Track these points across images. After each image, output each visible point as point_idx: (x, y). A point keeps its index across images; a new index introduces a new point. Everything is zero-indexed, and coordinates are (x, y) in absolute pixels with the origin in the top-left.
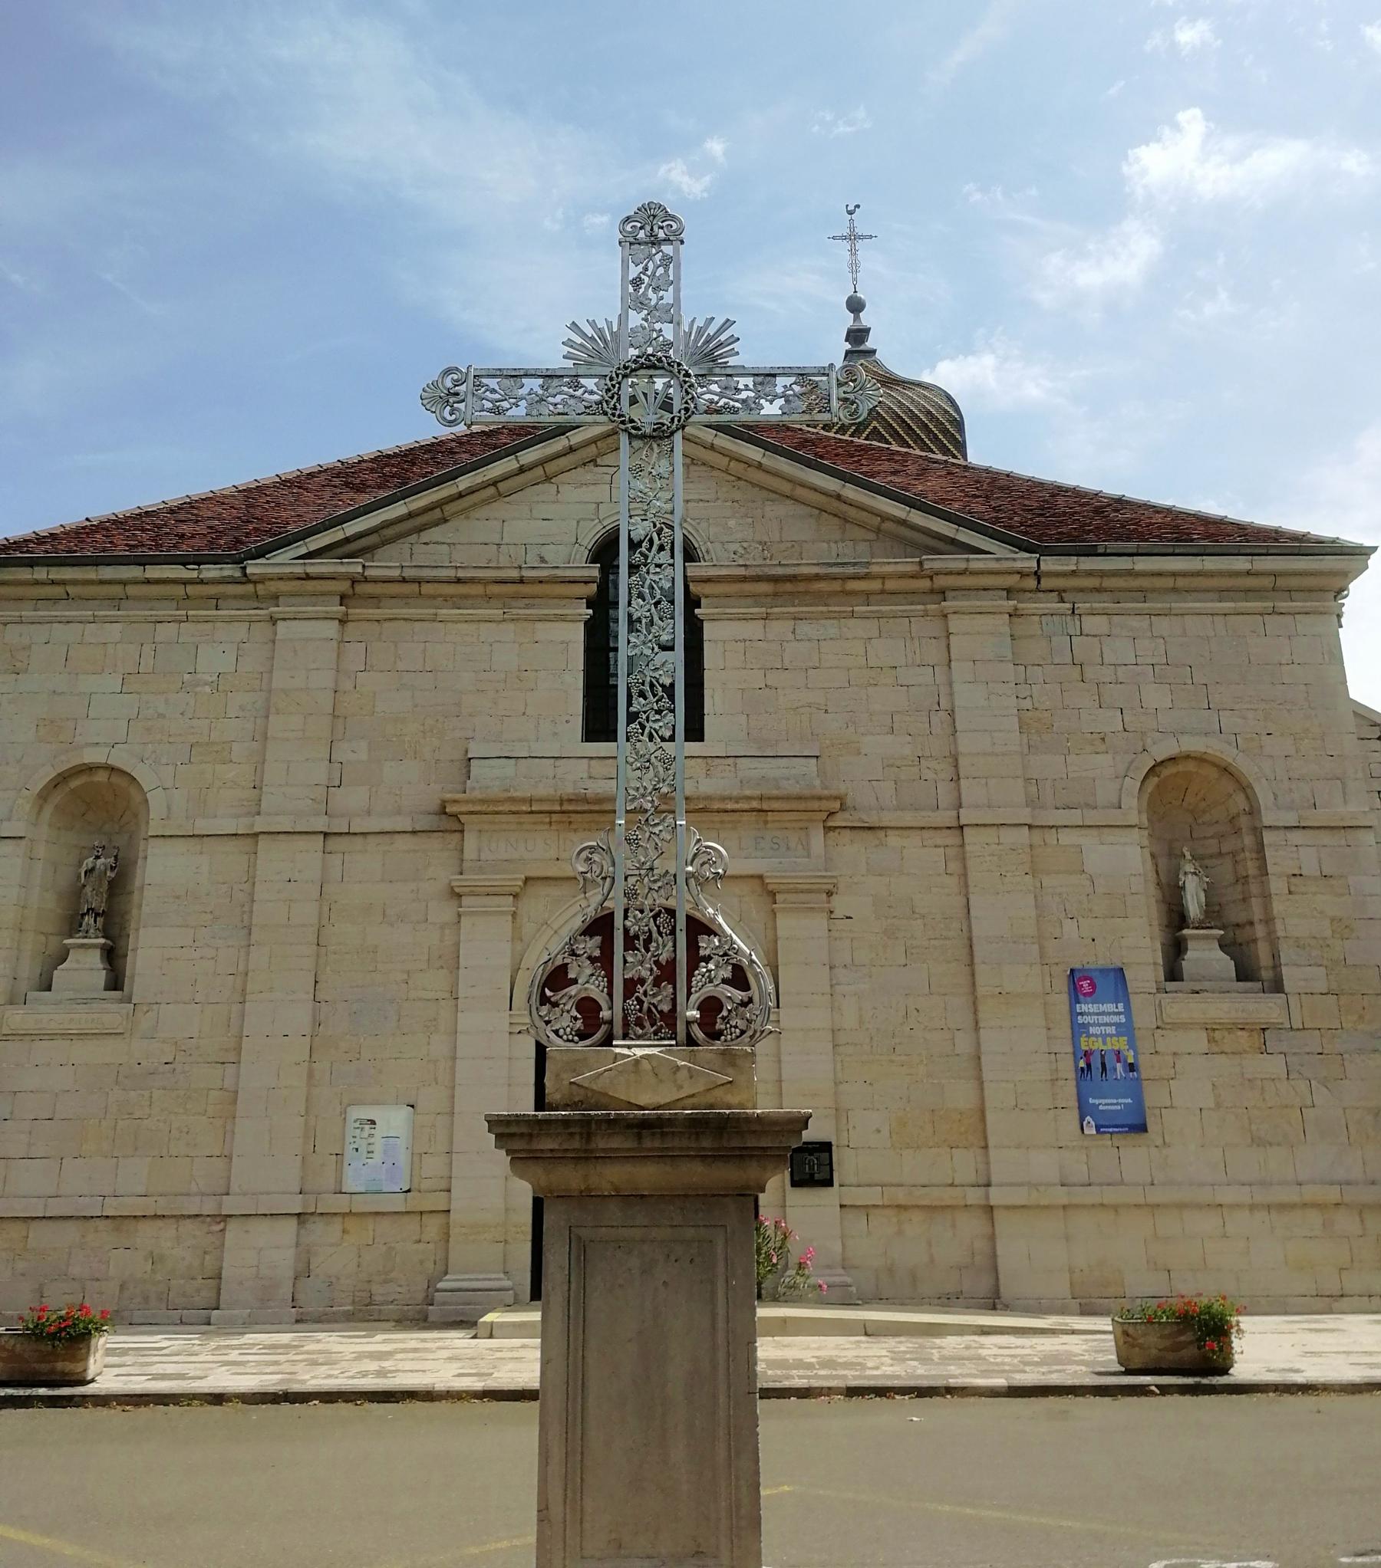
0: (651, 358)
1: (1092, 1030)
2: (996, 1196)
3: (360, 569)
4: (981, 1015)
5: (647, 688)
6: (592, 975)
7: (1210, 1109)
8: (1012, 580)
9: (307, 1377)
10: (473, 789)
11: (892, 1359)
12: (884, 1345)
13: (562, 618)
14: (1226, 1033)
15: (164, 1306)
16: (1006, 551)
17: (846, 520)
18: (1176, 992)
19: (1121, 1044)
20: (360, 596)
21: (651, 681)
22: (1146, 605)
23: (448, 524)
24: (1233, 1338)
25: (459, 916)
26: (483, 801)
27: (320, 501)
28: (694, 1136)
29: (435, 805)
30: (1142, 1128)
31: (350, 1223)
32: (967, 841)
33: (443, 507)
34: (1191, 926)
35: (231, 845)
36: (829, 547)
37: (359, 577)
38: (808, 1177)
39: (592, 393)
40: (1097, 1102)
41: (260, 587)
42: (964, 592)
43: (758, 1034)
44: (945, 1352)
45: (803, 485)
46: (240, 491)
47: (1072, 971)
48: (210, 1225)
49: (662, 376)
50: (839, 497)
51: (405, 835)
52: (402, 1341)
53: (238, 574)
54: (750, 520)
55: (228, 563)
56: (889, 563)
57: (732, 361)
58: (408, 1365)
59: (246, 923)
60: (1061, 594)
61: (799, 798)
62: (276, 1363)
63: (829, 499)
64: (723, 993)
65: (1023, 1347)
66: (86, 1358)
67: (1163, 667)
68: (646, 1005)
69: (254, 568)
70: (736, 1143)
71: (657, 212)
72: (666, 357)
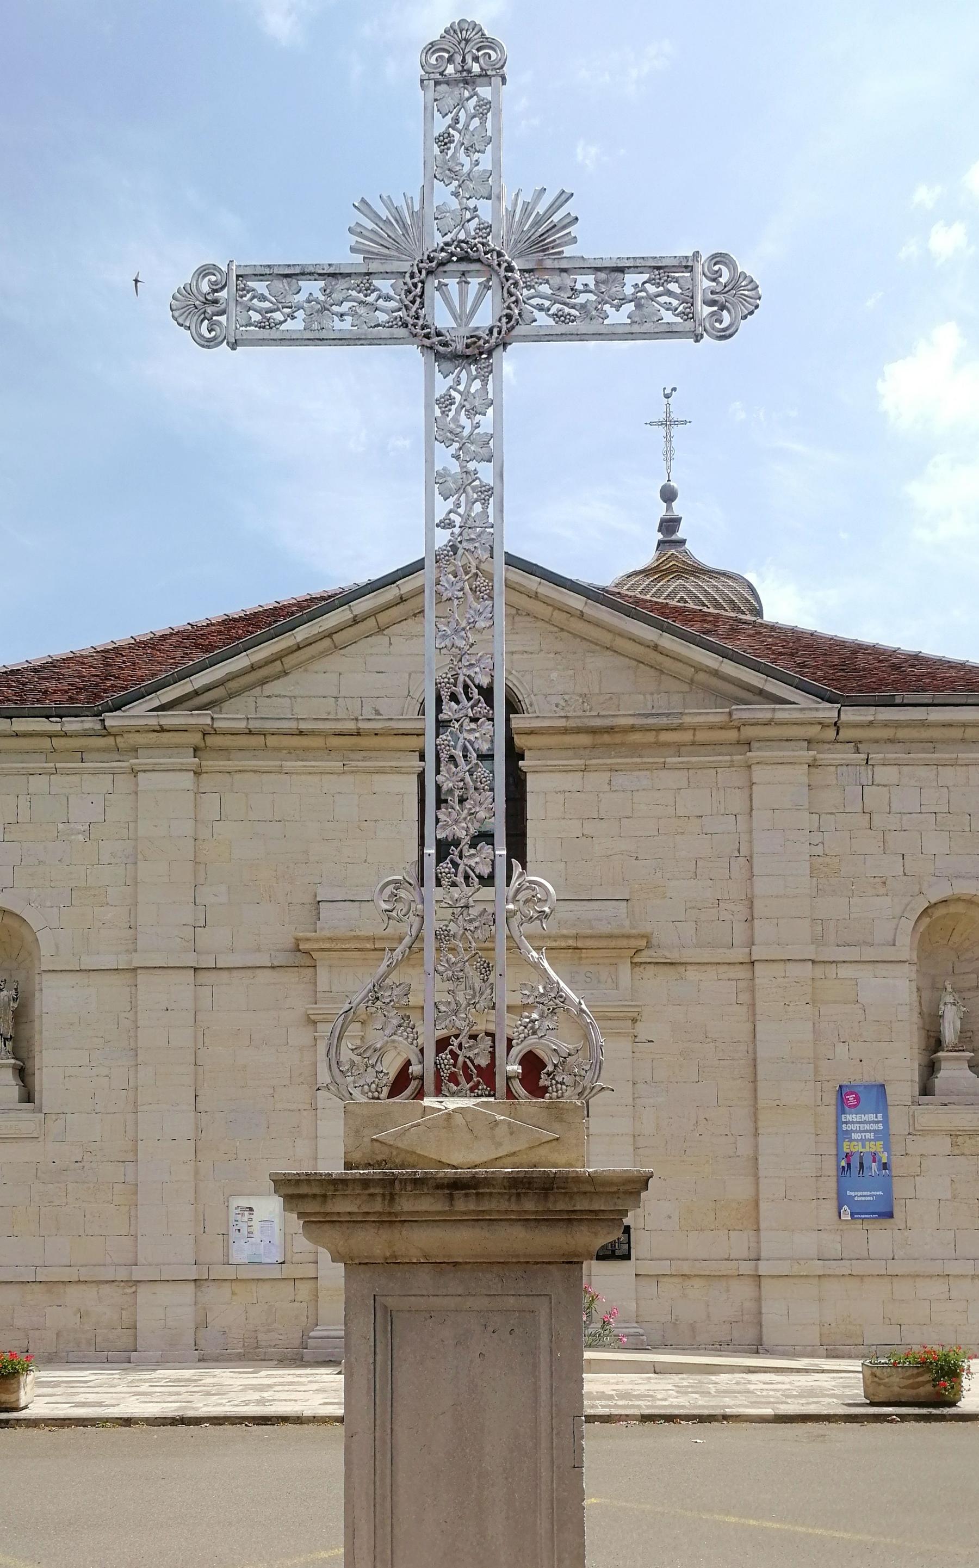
0: (464, 245)
1: (854, 1136)
2: (764, 1268)
3: (209, 721)
4: (760, 1124)
5: (460, 689)
6: (400, 1026)
7: (947, 1200)
8: (814, 731)
9: (201, 1405)
10: (323, 929)
11: (677, 1392)
12: (670, 1381)
13: (397, 771)
14: (967, 1138)
15: (93, 1348)
16: (810, 702)
17: (662, 672)
18: (927, 1104)
19: (878, 1147)
20: (212, 749)
21: (465, 681)
22: (936, 755)
23: (290, 676)
24: (963, 1379)
25: (316, 1040)
26: (330, 939)
27: (172, 661)
28: (513, 1199)
29: (290, 943)
30: (890, 1215)
31: (238, 1288)
32: (757, 974)
33: (283, 659)
34: (946, 1049)
35: (115, 979)
36: (645, 698)
37: (208, 729)
38: (610, 1253)
39: (388, 298)
40: (853, 1194)
41: (119, 739)
42: (768, 743)
43: (588, 1091)
44: (719, 1387)
45: (621, 634)
46: (98, 652)
47: (841, 1087)
48: (124, 1288)
49: (478, 273)
50: (656, 647)
51: (265, 970)
52: (282, 1376)
53: (98, 726)
54: (571, 672)
55: (87, 716)
56: (700, 714)
57: (568, 251)
58: (283, 1396)
59: (133, 1044)
60: (856, 745)
61: (611, 937)
62: (178, 1394)
63: (647, 650)
64: (548, 1046)
65: (783, 1384)
66: (18, 1390)
67: (945, 815)
68: (461, 1059)
69: (112, 720)
70: (561, 1206)
71: (470, 35)
72: (483, 244)
